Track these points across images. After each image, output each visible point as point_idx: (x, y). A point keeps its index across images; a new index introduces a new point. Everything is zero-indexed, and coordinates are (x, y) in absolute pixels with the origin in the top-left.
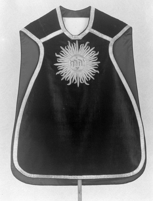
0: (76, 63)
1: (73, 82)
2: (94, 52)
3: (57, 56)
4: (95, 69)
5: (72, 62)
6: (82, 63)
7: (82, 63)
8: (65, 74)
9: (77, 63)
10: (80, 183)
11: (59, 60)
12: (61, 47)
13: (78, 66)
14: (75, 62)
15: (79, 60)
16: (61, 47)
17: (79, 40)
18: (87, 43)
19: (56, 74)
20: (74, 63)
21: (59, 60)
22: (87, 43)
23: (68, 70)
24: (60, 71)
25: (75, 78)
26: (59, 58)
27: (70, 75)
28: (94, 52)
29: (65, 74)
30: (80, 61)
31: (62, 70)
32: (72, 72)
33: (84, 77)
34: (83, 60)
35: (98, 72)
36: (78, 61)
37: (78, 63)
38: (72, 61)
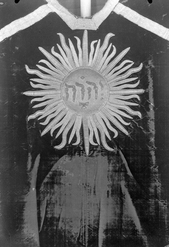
0: (81, 92)
1: (70, 142)
2: (129, 63)
3: (30, 71)
4: (133, 108)
5: (70, 90)
6: (96, 92)
7: (96, 92)
8: (52, 120)
9: (83, 91)
10: (136, 113)
11: (35, 83)
12: (41, 49)
13: (84, 101)
14: (78, 89)
15: (89, 83)
16: (41, 49)
17: (90, 32)
18: (110, 35)
19: (25, 117)
20: (74, 90)
21: (35, 83)
22: (110, 35)
23: (59, 110)
24: (38, 113)
25: (76, 130)
26: (35, 76)
27: (65, 122)
28: (129, 63)
29: (52, 120)
30: (92, 87)
31: (42, 108)
32: (70, 114)
33: (99, 127)
34: (100, 83)
35: (139, 114)
36: (87, 86)
37: (87, 91)
38: (70, 87)
